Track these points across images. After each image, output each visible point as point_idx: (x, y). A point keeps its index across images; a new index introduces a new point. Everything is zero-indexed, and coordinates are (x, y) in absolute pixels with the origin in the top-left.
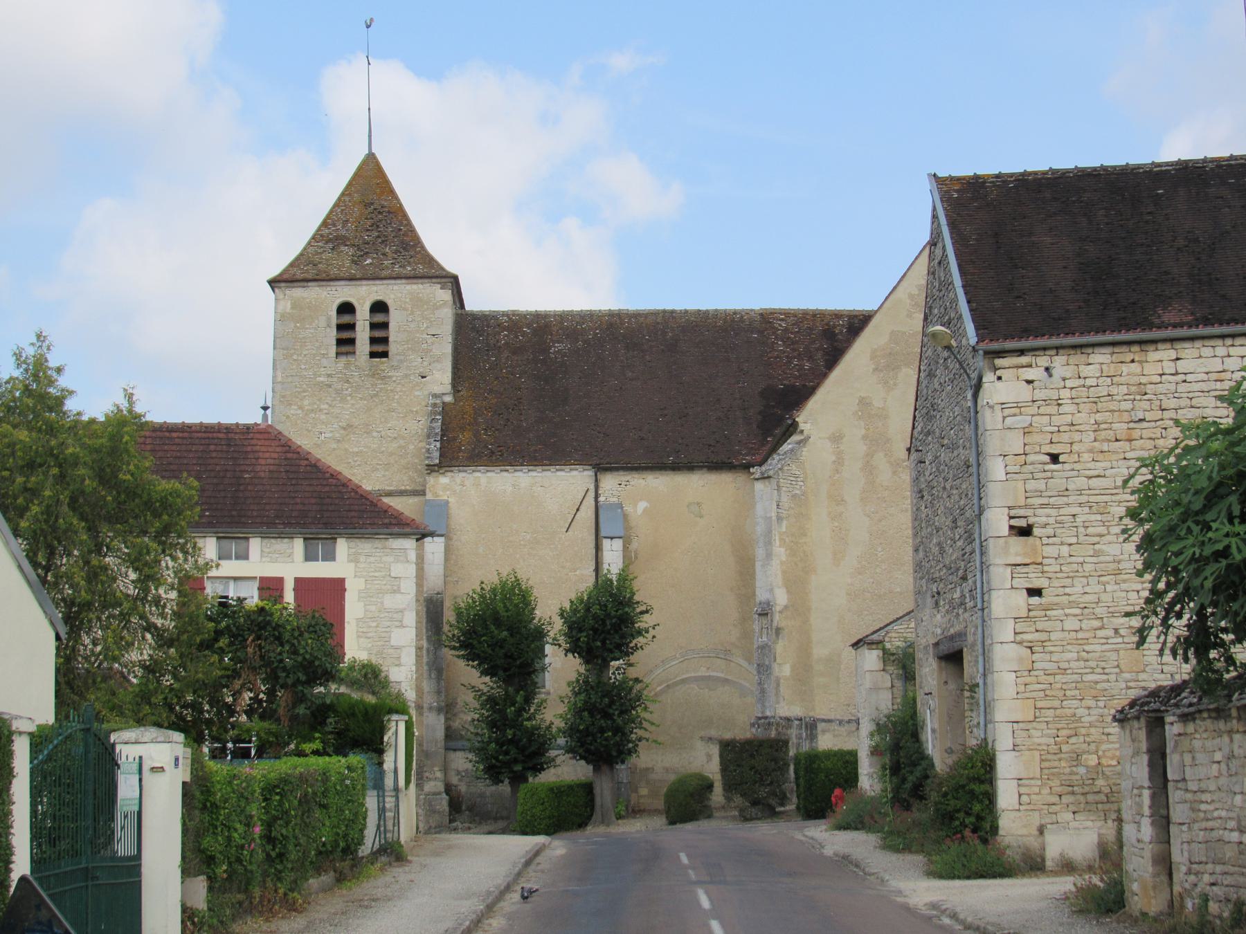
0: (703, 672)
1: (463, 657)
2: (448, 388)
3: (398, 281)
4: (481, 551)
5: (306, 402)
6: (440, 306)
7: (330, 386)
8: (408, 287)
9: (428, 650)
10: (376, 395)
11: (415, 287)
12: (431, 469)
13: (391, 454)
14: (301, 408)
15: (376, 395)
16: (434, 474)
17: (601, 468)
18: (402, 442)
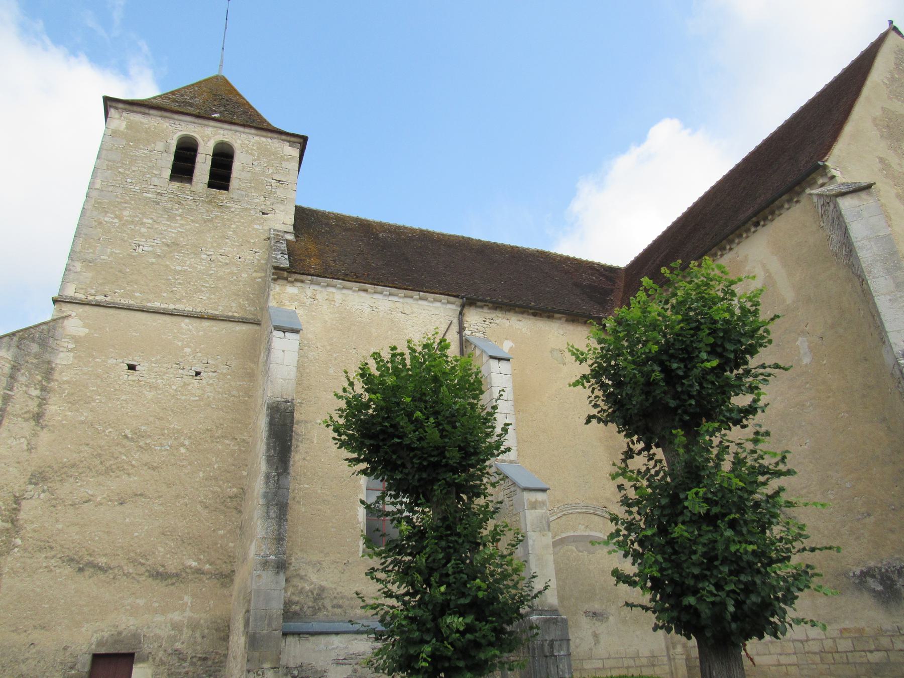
0: (581, 531)
1: (364, 472)
2: (291, 229)
3: (247, 130)
4: (331, 371)
5: (126, 213)
6: (288, 160)
7: (158, 204)
8: (257, 138)
9: (267, 476)
10: (211, 221)
11: (263, 139)
12: (280, 274)
13: (220, 279)
14: (120, 218)
15: (211, 221)
16: (281, 282)
17: (470, 302)
18: (234, 269)
